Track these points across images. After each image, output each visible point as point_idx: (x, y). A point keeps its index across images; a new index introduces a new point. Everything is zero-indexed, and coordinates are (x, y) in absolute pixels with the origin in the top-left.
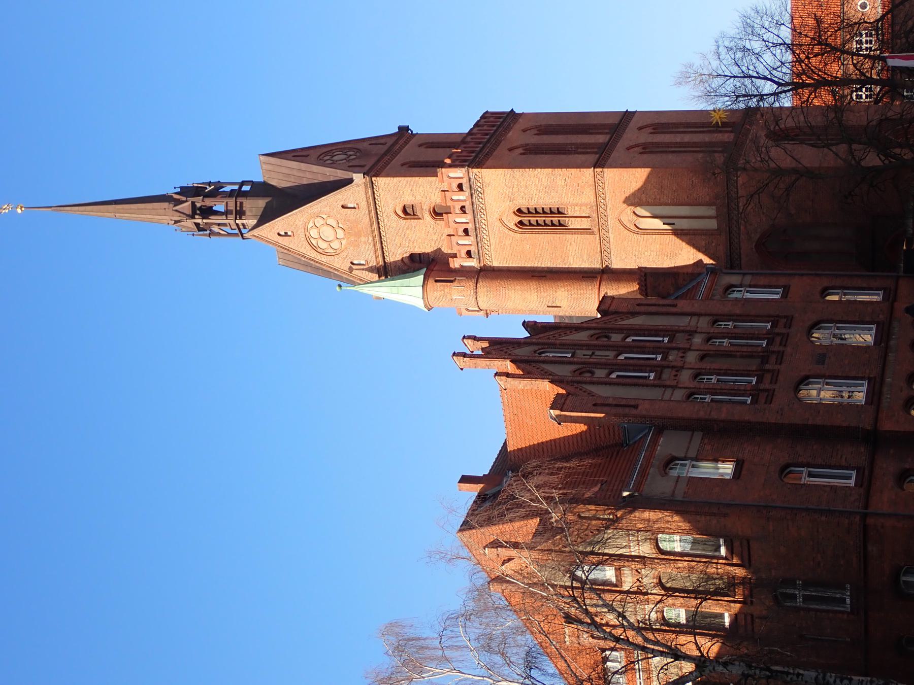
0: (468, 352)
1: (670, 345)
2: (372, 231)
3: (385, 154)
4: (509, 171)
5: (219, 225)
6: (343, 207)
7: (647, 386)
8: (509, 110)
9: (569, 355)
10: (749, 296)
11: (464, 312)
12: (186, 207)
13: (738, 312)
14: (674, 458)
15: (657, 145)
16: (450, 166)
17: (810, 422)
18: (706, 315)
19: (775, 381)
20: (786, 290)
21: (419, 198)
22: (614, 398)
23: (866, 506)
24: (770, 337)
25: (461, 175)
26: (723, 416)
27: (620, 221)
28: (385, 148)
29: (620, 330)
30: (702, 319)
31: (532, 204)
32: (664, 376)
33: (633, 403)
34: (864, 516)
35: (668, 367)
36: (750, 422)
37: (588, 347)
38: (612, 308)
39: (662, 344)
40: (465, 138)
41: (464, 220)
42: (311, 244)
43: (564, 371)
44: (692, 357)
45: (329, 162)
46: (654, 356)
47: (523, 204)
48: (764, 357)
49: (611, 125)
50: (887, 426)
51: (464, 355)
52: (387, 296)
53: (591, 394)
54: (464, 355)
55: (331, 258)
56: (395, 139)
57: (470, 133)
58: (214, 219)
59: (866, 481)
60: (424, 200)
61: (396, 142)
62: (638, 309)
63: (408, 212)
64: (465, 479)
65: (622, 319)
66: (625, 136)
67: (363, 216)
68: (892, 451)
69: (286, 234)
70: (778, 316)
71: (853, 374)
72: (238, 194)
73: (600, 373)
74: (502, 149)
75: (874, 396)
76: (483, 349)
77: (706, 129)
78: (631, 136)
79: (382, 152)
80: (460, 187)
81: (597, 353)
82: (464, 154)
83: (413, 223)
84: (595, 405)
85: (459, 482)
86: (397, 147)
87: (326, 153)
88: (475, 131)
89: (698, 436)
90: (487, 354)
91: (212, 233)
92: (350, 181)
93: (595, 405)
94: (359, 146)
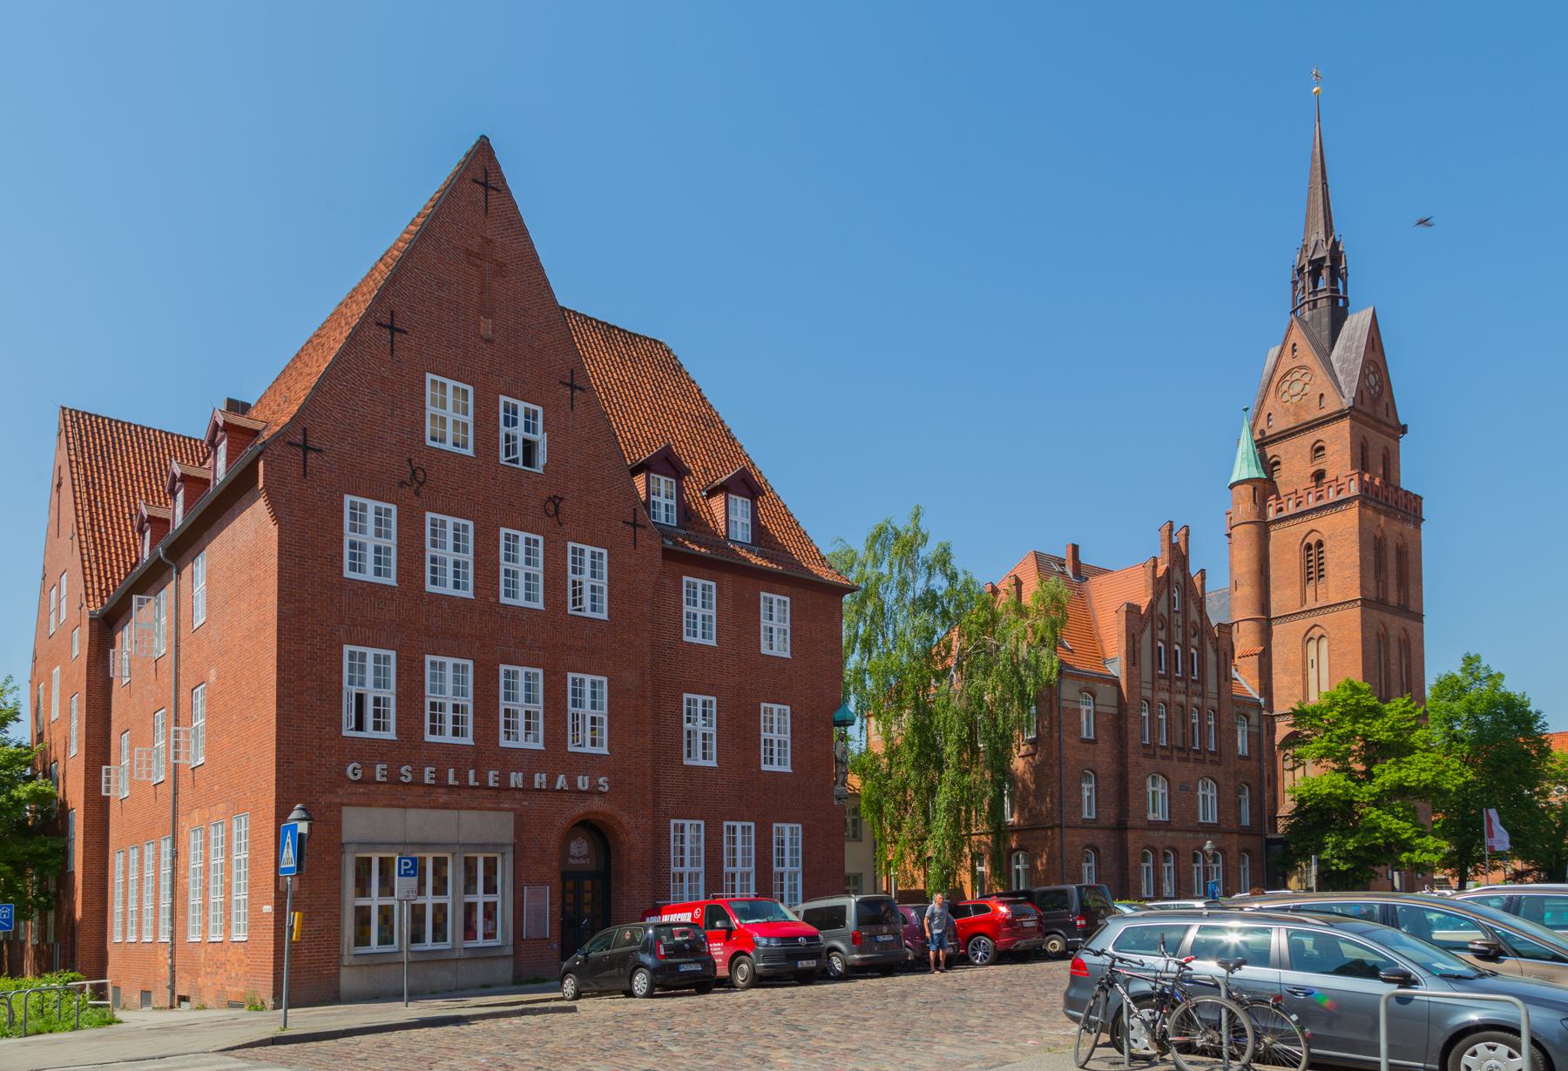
0: (1174, 533)
1: (1189, 681)
5: (1304, 287)
7: (1153, 670)
13: (1223, 726)
15: (1387, 645)
16: (1361, 479)
17: (1130, 785)
18: (1219, 704)
19: (1163, 758)
20: (1247, 758)
22: (1140, 648)
23: (1067, 827)
24: (1203, 751)
26: (1130, 726)
28: (1384, 418)
30: (1216, 701)
31: (1327, 554)
32: (1162, 681)
33: (1137, 662)
34: (1060, 826)
36: (1127, 745)
37: (1185, 622)
42: (1286, 375)
43: (1162, 608)
45: (1367, 372)
46: (1180, 670)
47: (1327, 547)
50: (1131, 836)
51: (1171, 530)
53: (1142, 631)
54: (1171, 530)
57: (1398, 488)
59: (1087, 825)
60: (1329, 463)
63: (1318, 450)
64: (1075, 548)
69: (1294, 351)
71: (1173, 811)
73: (1162, 634)
75: (1156, 826)
77: (1404, 680)
78: (1395, 624)
80: (1320, 498)
81: (1180, 630)
82: (1375, 488)
83: (1308, 458)
86: (1385, 428)
88: (1400, 493)
89: (1114, 711)
90: (1174, 547)
93: (1133, 635)
94: (1385, 393)
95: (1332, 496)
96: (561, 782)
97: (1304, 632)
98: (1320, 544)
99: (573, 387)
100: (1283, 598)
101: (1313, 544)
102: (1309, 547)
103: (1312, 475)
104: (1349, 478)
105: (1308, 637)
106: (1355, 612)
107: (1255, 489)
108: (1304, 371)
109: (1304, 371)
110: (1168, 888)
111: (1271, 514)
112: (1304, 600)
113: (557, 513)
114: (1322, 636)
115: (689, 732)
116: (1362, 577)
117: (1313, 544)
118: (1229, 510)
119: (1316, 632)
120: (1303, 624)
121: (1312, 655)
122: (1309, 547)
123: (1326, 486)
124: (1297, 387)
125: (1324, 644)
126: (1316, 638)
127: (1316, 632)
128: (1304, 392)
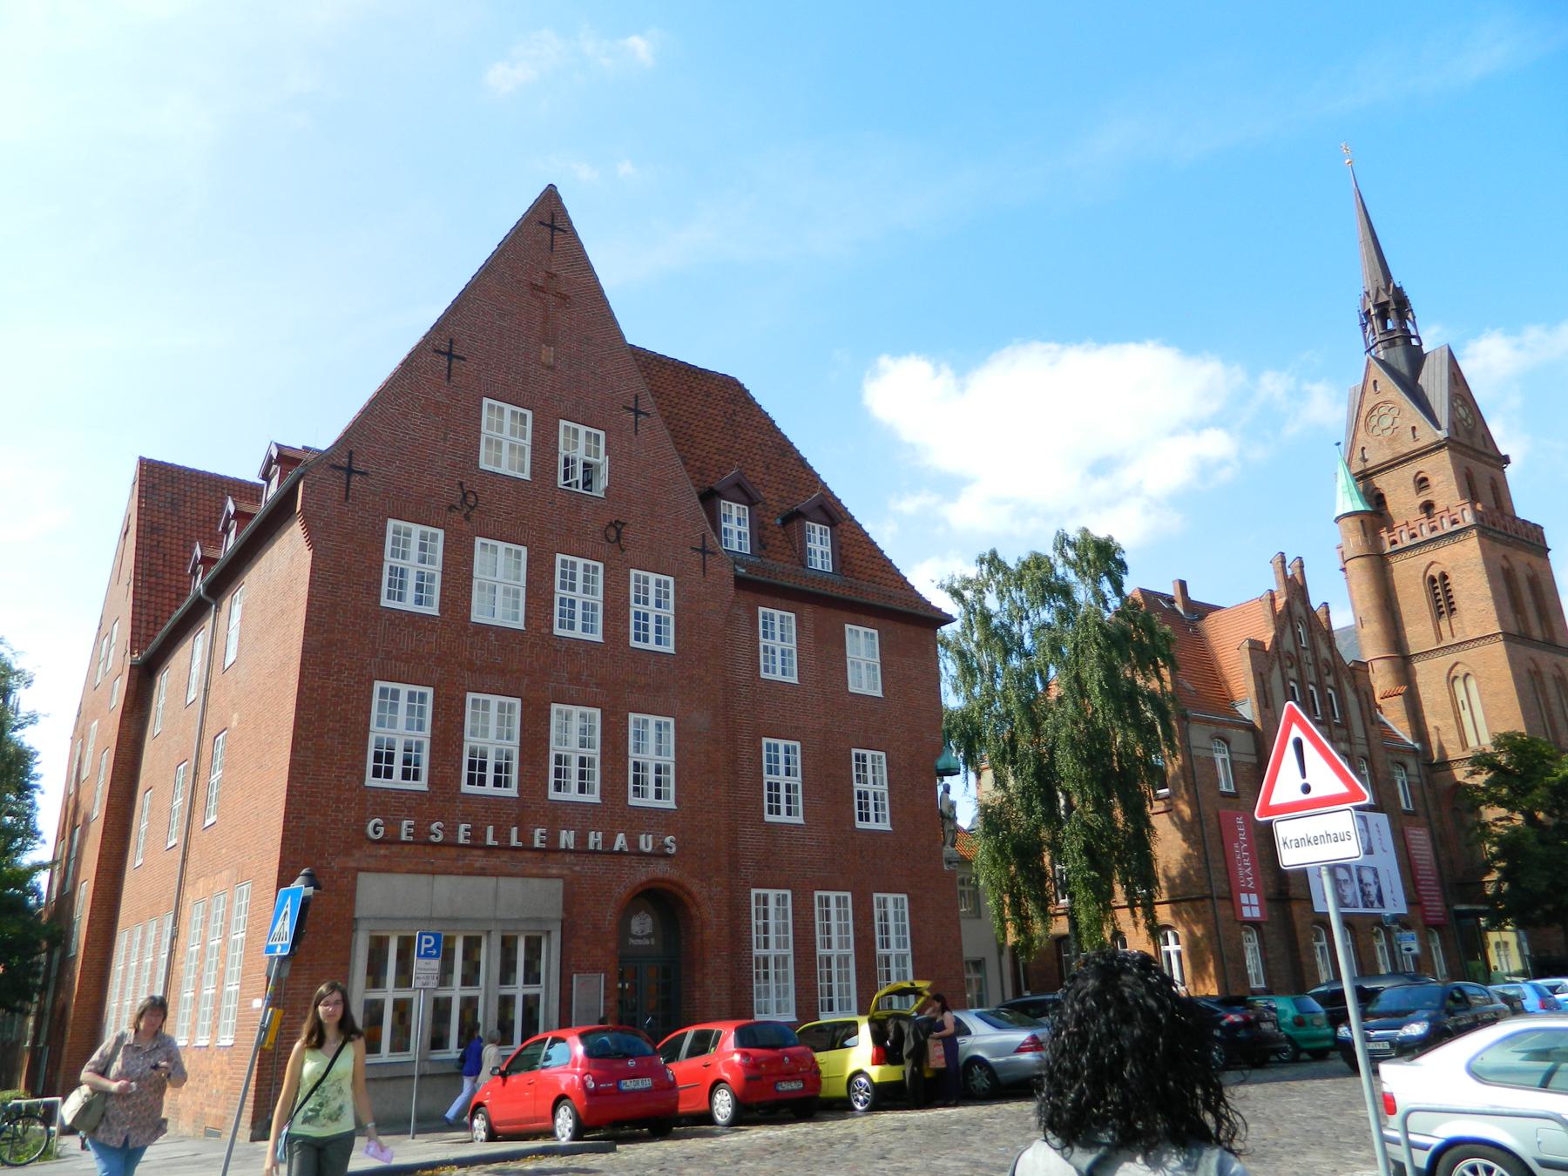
0: (1287, 565)
1: (1332, 724)
2: (1397, 458)
5: (1373, 329)
8: (1549, 547)
9: (1304, 645)
10: (1399, 785)
12: (1383, 298)
13: (1379, 776)
14: (1228, 743)
18: (1369, 750)
21: (1437, 489)
23: (1220, 898)
25: (1467, 520)
27: (1457, 664)
28: (1482, 449)
29: (1338, 681)
30: (1366, 748)
33: (1270, 703)
37: (1316, 659)
38: (1357, 673)
39: (1331, 717)
40: (1507, 515)
41: (1424, 532)
42: (1372, 410)
43: (1288, 644)
45: (1455, 404)
53: (1270, 670)
56: (1494, 454)
57: (1515, 518)
58: (1377, 323)
60: (1436, 494)
61: (1490, 457)
62: (1362, 693)
63: (1422, 483)
64: (1183, 585)
65: (1349, 682)
66: (1544, 653)
67: (1408, 446)
68: (1275, 914)
72: (1407, 337)
73: (1293, 673)
74: (1501, 550)
76: (1293, 576)
79: (1477, 447)
81: (1312, 668)
83: (1412, 490)
84: (1261, 674)
86: (1486, 459)
91: (1364, 326)
92: (1438, 427)
97: (1446, 671)
98: (1444, 577)
100: (1418, 633)
103: (1421, 506)
104: (1460, 508)
105: (1452, 675)
106: (1499, 649)
107: (1362, 521)
108: (1390, 406)
109: (1390, 406)
112: (1440, 637)
121: (1461, 696)
122: (1433, 580)
124: (1387, 422)
126: (1461, 676)
127: (1460, 671)
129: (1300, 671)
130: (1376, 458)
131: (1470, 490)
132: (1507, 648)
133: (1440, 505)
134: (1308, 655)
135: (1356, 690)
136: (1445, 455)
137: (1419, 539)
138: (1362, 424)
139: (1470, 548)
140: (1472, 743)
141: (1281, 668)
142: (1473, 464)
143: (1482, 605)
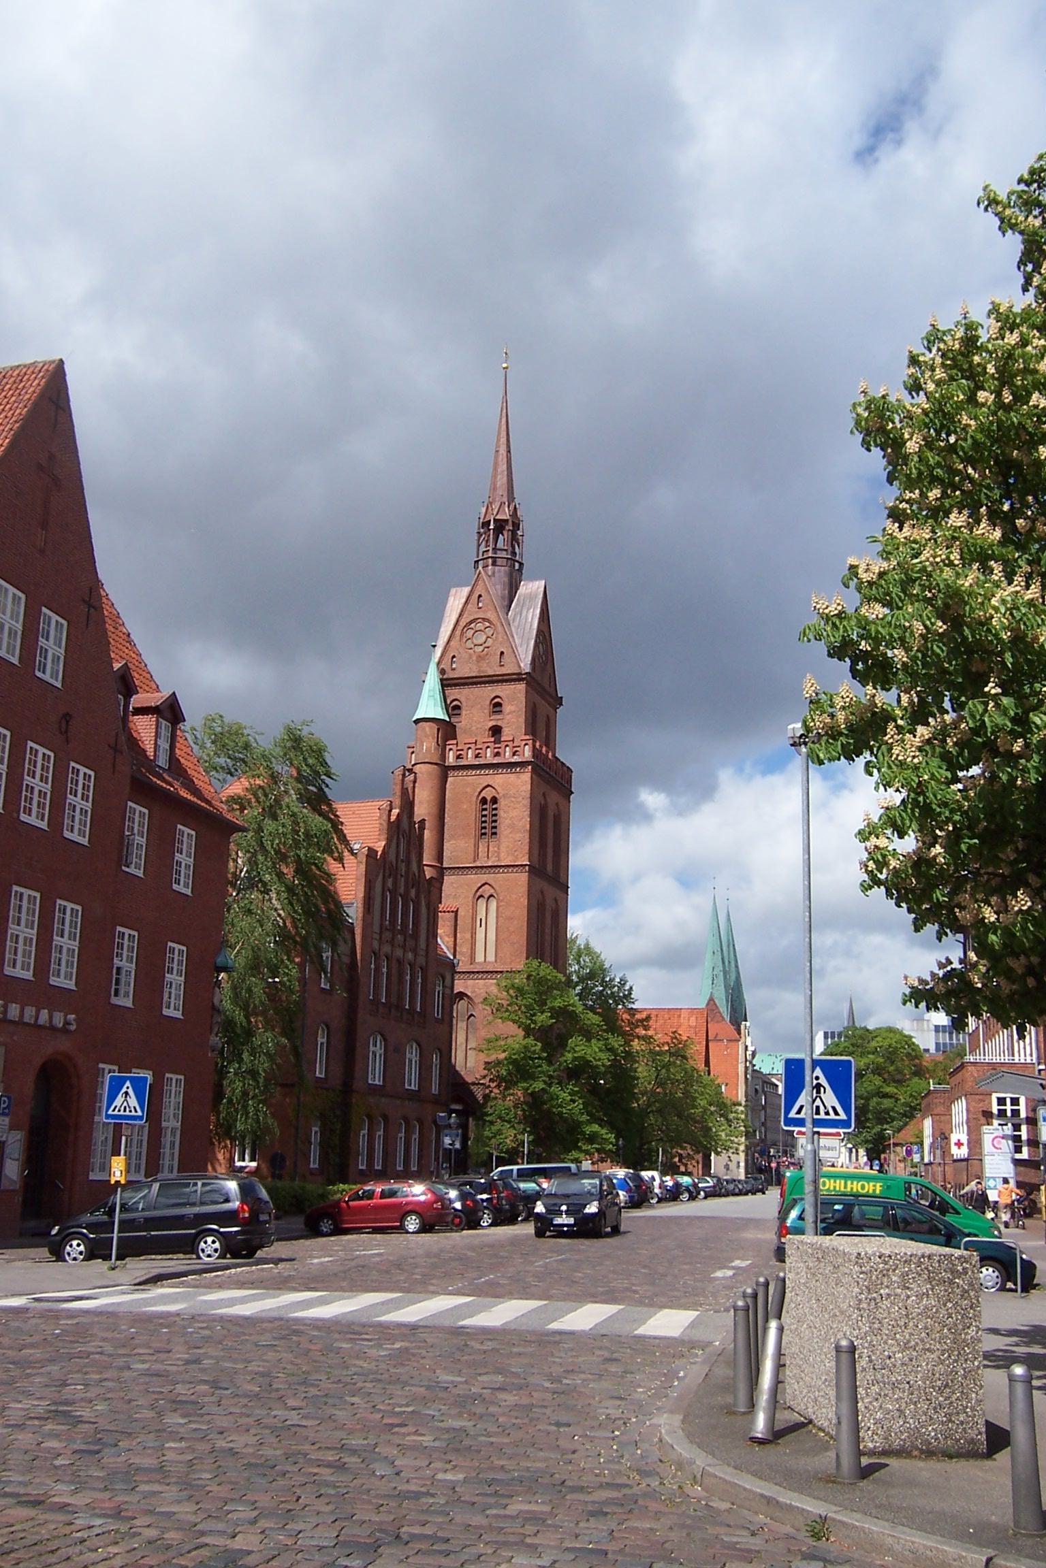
2: (482, 677)
3: (543, 688)
4: (528, 795)
6: (502, 653)
11: (411, 750)
16: (534, 746)
21: (508, 717)
28: (547, 687)
35: (393, 935)
37: (407, 872)
42: (471, 622)
44: (399, 953)
47: (502, 803)
48: (399, 1007)
49: (559, 877)
52: (427, 687)
53: (377, 876)
55: (458, 638)
60: (505, 721)
61: (550, 695)
70: (425, 1016)
75: (374, 1090)
80: (497, 754)
85: (174, 693)
87: (544, 637)
94: (549, 666)
95: (507, 756)
96: (44, 1015)
97: (474, 891)
98: (494, 800)
99: (90, 606)
101: (489, 799)
102: (484, 801)
103: (490, 729)
104: (524, 743)
105: (478, 894)
106: (523, 877)
108: (487, 624)
110: (247, 1157)
111: (451, 759)
112: (476, 857)
113: (66, 731)
114: (491, 896)
115: (119, 969)
116: (530, 842)
117: (489, 799)
118: (412, 744)
119: (487, 890)
120: (476, 879)
121: (481, 914)
122: (484, 801)
123: (503, 745)
124: (481, 638)
125: (493, 904)
126: (486, 896)
127: (487, 890)
128: (486, 645)
129: (395, 883)
130: (464, 669)
131: (532, 727)
132: (529, 877)
133: (506, 735)
134: (403, 867)
135: (428, 908)
136: (522, 687)
137: (482, 761)
138: (458, 632)
139: (522, 782)
140: (480, 958)
141: (384, 876)
142: (538, 699)
143: (518, 836)
